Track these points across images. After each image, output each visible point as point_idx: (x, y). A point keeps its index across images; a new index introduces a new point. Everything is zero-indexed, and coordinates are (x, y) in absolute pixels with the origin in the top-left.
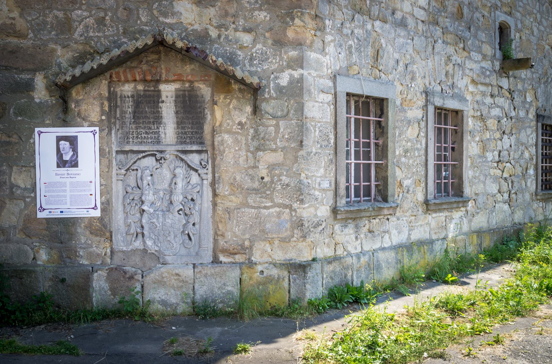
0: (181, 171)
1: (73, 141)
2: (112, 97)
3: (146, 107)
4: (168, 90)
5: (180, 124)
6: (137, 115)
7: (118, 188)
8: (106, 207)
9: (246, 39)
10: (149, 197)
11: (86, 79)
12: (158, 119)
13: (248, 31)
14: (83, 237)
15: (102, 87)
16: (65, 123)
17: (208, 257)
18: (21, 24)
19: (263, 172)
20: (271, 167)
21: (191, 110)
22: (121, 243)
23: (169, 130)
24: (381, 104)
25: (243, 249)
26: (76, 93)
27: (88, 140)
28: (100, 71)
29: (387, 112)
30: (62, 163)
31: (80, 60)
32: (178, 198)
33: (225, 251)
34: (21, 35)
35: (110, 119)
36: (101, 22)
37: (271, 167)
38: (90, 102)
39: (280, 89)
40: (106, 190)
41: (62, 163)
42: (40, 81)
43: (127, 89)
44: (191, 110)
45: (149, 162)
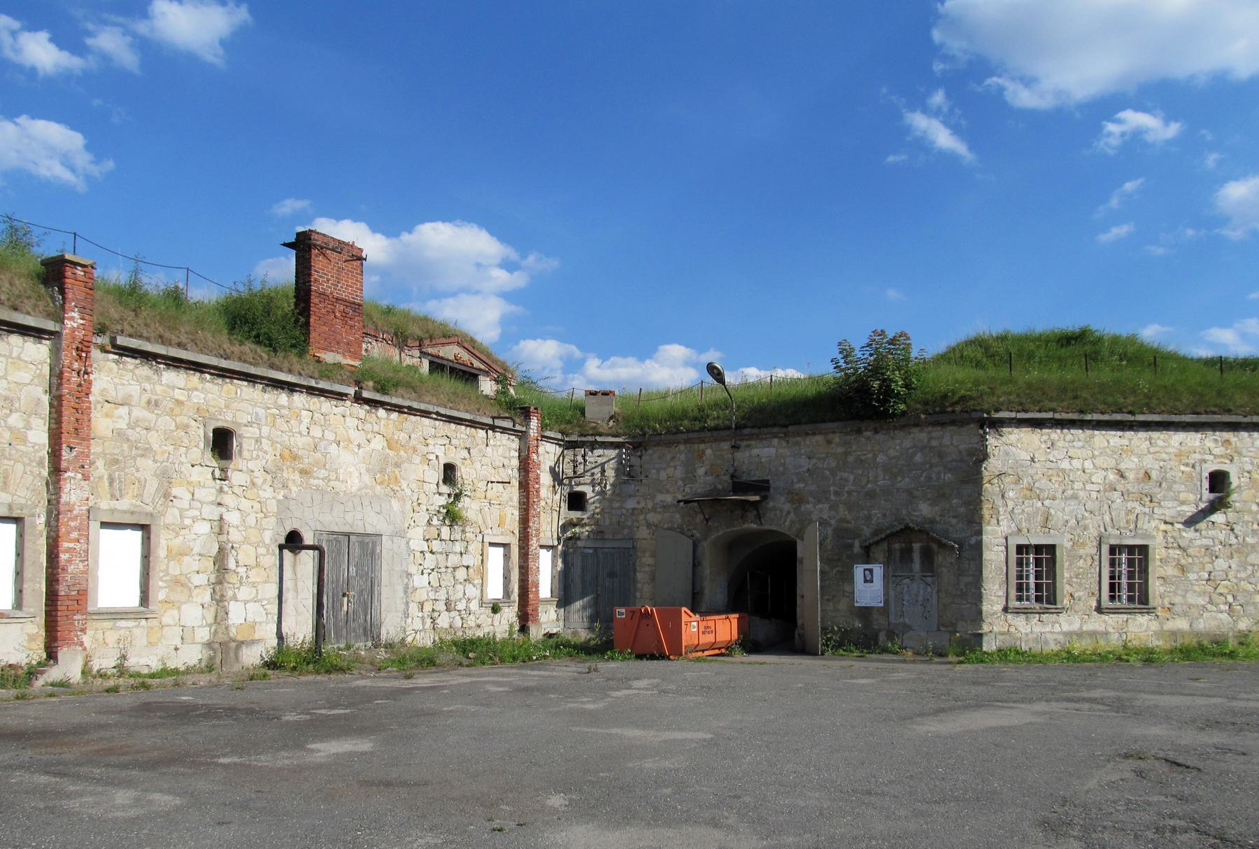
0: (922, 586)
1: (871, 571)
2: (890, 551)
3: (906, 554)
4: (916, 546)
5: (922, 563)
6: (902, 558)
7: (892, 593)
8: (886, 602)
9: (954, 521)
10: (906, 598)
11: (877, 543)
12: (911, 560)
13: (955, 517)
14: (875, 615)
15: (885, 545)
16: (867, 563)
17: (935, 628)
18: (849, 517)
19: (962, 586)
20: (966, 585)
21: (927, 556)
22: (892, 619)
23: (917, 565)
24: (1051, 549)
25: (953, 625)
26: (873, 549)
27: (878, 570)
28: (882, 540)
29: (553, 577)
30: (866, 581)
31: (875, 533)
32: (920, 599)
33: (943, 625)
34: (848, 522)
35: (887, 564)
36: (884, 515)
37: (966, 585)
38: (879, 552)
39: (970, 546)
40: (886, 594)
41: (866, 581)
42: (857, 543)
43: (897, 546)
44: (927, 556)
45: (907, 581)
